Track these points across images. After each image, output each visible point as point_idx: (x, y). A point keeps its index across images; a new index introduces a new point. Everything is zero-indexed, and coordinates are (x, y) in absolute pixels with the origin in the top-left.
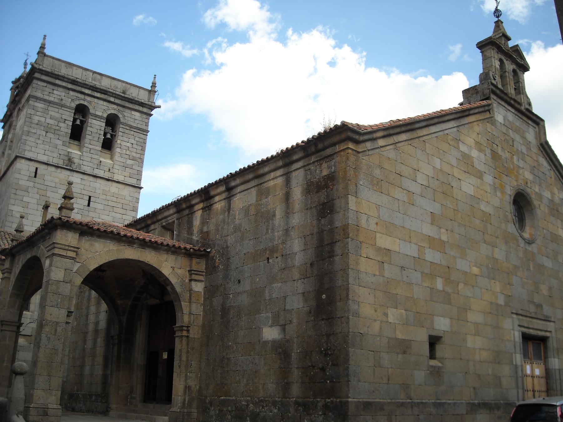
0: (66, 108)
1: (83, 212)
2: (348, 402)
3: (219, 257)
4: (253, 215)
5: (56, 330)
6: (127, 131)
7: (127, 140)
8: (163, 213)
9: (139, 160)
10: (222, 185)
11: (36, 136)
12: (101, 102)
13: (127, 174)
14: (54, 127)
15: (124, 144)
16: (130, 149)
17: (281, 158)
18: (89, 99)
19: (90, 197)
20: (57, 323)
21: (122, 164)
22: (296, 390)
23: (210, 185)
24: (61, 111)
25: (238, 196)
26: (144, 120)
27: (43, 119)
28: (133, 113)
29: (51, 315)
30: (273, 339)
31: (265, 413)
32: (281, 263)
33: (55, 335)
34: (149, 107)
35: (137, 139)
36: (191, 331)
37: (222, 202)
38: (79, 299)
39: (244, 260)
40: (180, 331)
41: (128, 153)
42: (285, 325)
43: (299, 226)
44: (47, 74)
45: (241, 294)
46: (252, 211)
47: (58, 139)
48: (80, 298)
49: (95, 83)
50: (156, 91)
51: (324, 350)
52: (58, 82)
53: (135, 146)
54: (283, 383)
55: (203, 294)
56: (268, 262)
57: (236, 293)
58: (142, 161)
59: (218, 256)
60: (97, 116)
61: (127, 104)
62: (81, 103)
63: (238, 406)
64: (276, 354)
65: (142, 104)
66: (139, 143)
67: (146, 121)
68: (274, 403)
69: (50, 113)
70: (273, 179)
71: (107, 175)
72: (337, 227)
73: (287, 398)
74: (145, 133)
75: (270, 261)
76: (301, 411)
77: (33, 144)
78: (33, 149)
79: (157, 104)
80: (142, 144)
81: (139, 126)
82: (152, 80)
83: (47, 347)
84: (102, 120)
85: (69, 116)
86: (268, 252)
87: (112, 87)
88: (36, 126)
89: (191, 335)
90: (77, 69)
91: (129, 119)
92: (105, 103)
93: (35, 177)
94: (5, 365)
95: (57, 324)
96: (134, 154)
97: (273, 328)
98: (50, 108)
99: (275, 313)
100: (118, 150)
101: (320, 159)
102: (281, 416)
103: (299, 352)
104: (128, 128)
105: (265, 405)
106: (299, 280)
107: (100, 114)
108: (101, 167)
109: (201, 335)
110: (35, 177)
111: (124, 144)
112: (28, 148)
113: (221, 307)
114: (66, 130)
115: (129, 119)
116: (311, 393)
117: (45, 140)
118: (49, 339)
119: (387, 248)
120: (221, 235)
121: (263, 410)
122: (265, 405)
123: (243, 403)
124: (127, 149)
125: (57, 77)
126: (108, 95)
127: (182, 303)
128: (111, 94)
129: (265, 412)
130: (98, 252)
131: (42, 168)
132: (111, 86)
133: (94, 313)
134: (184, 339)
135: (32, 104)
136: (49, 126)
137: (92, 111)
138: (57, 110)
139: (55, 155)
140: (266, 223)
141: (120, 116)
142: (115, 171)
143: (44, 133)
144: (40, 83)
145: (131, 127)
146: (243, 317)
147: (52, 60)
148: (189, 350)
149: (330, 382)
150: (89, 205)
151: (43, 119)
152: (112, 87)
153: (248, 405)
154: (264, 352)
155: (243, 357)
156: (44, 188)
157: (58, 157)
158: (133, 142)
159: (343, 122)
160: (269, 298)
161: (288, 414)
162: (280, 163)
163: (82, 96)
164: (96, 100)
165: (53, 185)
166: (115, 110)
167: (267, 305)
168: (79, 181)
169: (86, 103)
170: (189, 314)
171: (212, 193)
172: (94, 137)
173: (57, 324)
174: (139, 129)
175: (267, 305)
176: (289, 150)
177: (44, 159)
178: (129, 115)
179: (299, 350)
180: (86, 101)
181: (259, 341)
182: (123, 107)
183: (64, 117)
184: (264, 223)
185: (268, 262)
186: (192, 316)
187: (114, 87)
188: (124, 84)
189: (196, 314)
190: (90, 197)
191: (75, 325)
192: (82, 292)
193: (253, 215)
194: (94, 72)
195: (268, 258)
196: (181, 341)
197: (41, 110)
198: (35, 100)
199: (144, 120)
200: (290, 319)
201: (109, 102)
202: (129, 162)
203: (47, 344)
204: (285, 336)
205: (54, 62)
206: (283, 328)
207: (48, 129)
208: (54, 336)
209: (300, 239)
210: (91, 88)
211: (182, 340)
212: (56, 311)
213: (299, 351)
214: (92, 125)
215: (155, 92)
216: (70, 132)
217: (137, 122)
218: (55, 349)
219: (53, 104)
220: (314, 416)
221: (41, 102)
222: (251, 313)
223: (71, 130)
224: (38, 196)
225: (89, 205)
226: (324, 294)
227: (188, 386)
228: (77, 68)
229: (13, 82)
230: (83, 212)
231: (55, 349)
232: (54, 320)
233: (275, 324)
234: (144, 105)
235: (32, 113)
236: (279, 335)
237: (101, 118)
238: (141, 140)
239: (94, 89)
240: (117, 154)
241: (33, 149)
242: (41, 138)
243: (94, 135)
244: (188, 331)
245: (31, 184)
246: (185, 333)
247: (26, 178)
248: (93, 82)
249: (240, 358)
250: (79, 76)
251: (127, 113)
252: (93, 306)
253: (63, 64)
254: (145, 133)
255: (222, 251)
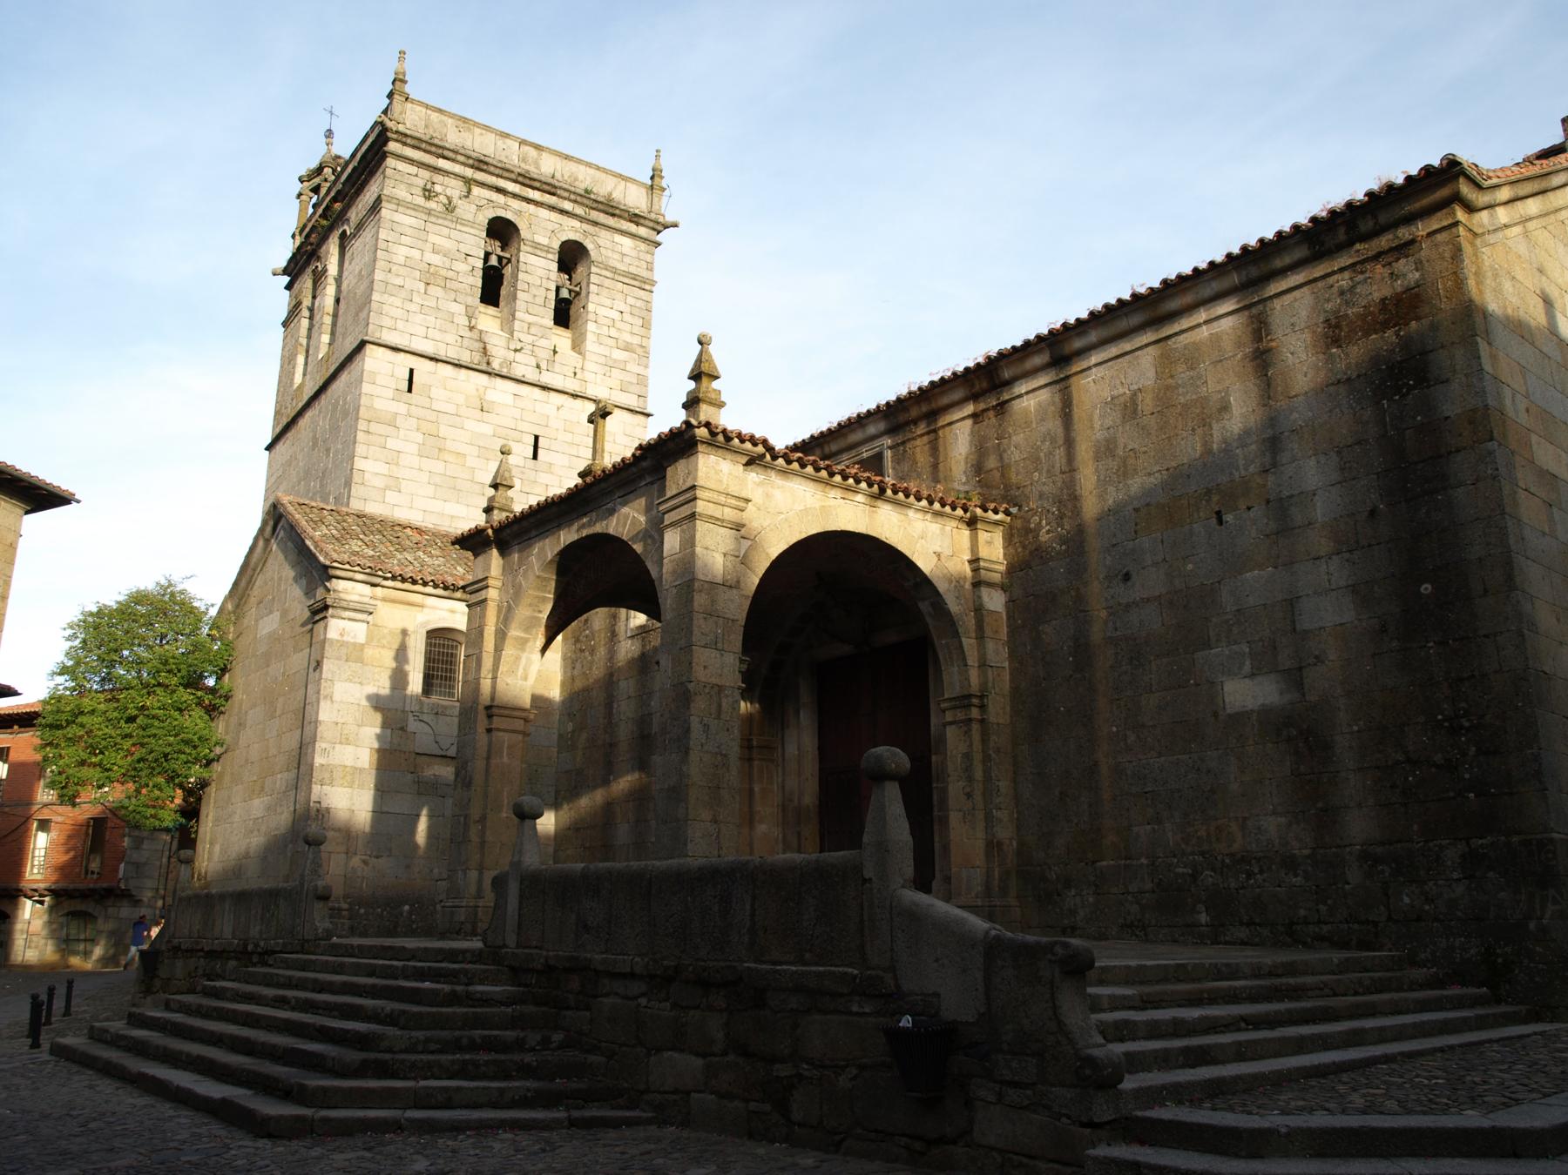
0: (467, 226)
1: (523, 473)
2: (1552, 840)
3: (1047, 525)
4: (1153, 413)
5: (720, 706)
6: (607, 283)
7: (608, 302)
8: (845, 436)
9: (640, 351)
10: (1039, 351)
11: (403, 294)
12: (544, 213)
13: (616, 384)
14: (443, 272)
15: (602, 311)
16: (618, 324)
17: (1236, 269)
18: (516, 204)
19: (537, 438)
20: (721, 688)
21: (603, 360)
22: (1359, 826)
23: (1002, 356)
24: (454, 234)
25: (1095, 373)
26: (642, 255)
27: (416, 254)
28: (618, 238)
29: (705, 667)
30: (1263, 705)
31: (1258, 890)
32: (1266, 521)
33: (718, 717)
34: (651, 224)
35: (631, 300)
36: (991, 708)
37: (1042, 391)
38: (574, 668)
39: (1136, 525)
40: (959, 710)
41: (613, 332)
42: (1300, 669)
43: (1313, 426)
44: (418, 143)
45: (1138, 605)
46: (1147, 403)
47: (455, 301)
48: (578, 665)
49: (527, 167)
50: (665, 186)
51: (1444, 720)
52: (442, 163)
53: (627, 317)
54: (1312, 812)
55: (1005, 617)
56: (1220, 522)
57: (1120, 604)
58: (645, 352)
59: (1044, 522)
60: (536, 246)
61: (602, 218)
62: (499, 214)
63: (1160, 880)
64: (1277, 743)
65: (635, 218)
66: (635, 311)
67: (648, 257)
68: (1290, 863)
69: (432, 238)
70: (1206, 322)
71: (571, 386)
72: (1447, 418)
73: (1331, 848)
74: (647, 287)
75: (1228, 518)
76: (1387, 874)
77: (399, 313)
78: (400, 325)
79: (669, 218)
80: (644, 314)
81: (633, 270)
82: (651, 163)
83: (706, 748)
84: (550, 256)
85: (476, 243)
86: (1215, 498)
87: (566, 178)
88: (402, 271)
89: (992, 719)
90: (482, 134)
91: (610, 254)
92: (554, 216)
93: (410, 390)
94: (505, 815)
95: (719, 693)
96: (628, 338)
97: (1260, 678)
98: (430, 227)
99: (1261, 644)
100: (591, 326)
101: (1364, 260)
102: (1316, 893)
103: (1358, 731)
104: (608, 274)
105: (1256, 871)
106: (1334, 557)
107: (545, 241)
108: (557, 368)
109: (1011, 716)
110: (410, 390)
111: (602, 311)
112: (387, 322)
113: (1071, 644)
114: (471, 280)
115: (610, 254)
116: (1415, 827)
117: (425, 303)
118: (706, 728)
119: (1551, 471)
120: (1048, 471)
121: (1252, 881)
122: (1256, 871)
123: (1180, 870)
124: (611, 324)
125: (440, 151)
126: (559, 196)
127: (963, 639)
128: (566, 194)
129: (1259, 887)
130: (782, 513)
131: (422, 366)
132: (563, 176)
133: (629, 697)
134: (975, 727)
135: (388, 217)
136: (432, 270)
137: (523, 234)
138: (446, 231)
139: (451, 338)
140: (1199, 431)
141: (589, 246)
142: (588, 376)
143: (422, 286)
144: (402, 166)
145: (614, 270)
146: (1150, 662)
147: (424, 110)
148: (991, 752)
149: (1476, 796)
150: (535, 457)
151: (416, 254)
152: (566, 178)
153: (1194, 877)
154: (1235, 741)
155: (1163, 759)
156: (432, 416)
157: (459, 344)
158: (622, 307)
159: (1451, 157)
160: (1236, 608)
161: (1340, 886)
162: (1235, 278)
163: (500, 198)
164: (532, 207)
165: (451, 409)
166: (576, 231)
167: (1232, 625)
168: (509, 400)
169: (509, 216)
170: (979, 667)
171: (1007, 374)
172: (535, 296)
173: (719, 693)
174: (634, 277)
175: (1232, 625)
176: (1285, 238)
177: (428, 348)
178: (609, 245)
179: (1357, 725)
180: (511, 210)
181: (1215, 714)
182: (596, 223)
183: (464, 249)
184: (1193, 430)
185: (1220, 522)
186: (990, 671)
187: (569, 177)
188: (591, 171)
189: (999, 665)
190: (537, 438)
191: (570, 729)
192: (582, 651)
193: (1153, 413)
194: (523, 142)
195: (1219, 513)
196: (968, 733)
197: (409, 231)
198: (394, 207)
199: (642, 255)
200: (1317, 653)
201: (563, 212)
202: (619, 355)
203: (703, 741)
204: (1304, 695)
205: (429, 116)
206: (1295, 678)
207: (430, 278)
208: (716, 721)
209: (1323, 459)
210: (520, 179)
211: (970, 730)
212: (716, 658)
213: (1356, 728)
214: (529, 268)
215: (663, 190)
216: (480, 285)
217: (627, 260)
218: (722, 755)
219: (435, 216)
220: (1435, 884)
221: (409, 212)
222: (1177, 649)
223: (483, 279)
224: (419, 438)
225: (535, 457)
226: (1426, 582)
227: (998, 842)
228: (484, 132)
229: (301, 180)
230: (523, 473)
231: (722, 755)
232: (714, 680)
233: (1265, 670)
234: (642, 221)
235: (389, 239)
236: (1281, 694)
237: (548, 252)
238: (639, 303)
239: (526, 180)
240: (590, 337)
241: (400, 325)
242: (416, 298)
243: (533, 290)
244: (982, 707)
245: (401, 408)
246: (975, 713)
247: (390, 394)
248: (523, 165)
249: (1152, 761)
250: (489, 151)
251: (604, 237)
252: (627, 679)
253: (450, 121)
254: (647, 287)
255: (1059, 510)
